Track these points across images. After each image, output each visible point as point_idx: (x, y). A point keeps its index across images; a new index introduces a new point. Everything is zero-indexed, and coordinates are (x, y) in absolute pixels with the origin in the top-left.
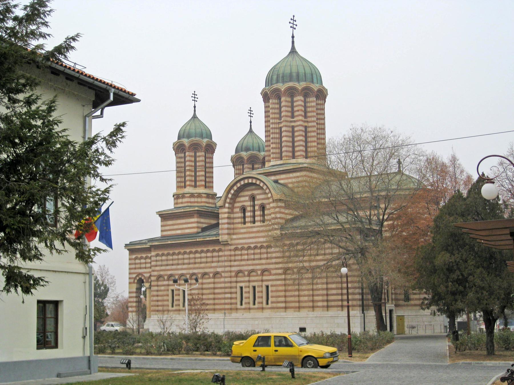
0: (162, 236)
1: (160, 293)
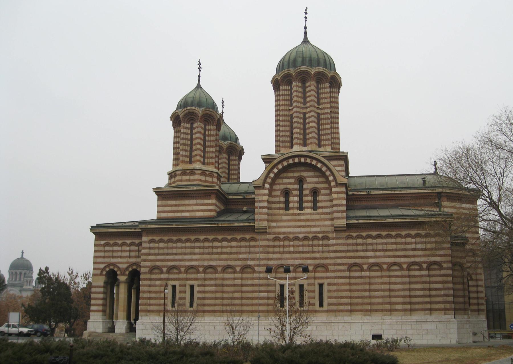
0: (158, 219)
1: (153, 289)
